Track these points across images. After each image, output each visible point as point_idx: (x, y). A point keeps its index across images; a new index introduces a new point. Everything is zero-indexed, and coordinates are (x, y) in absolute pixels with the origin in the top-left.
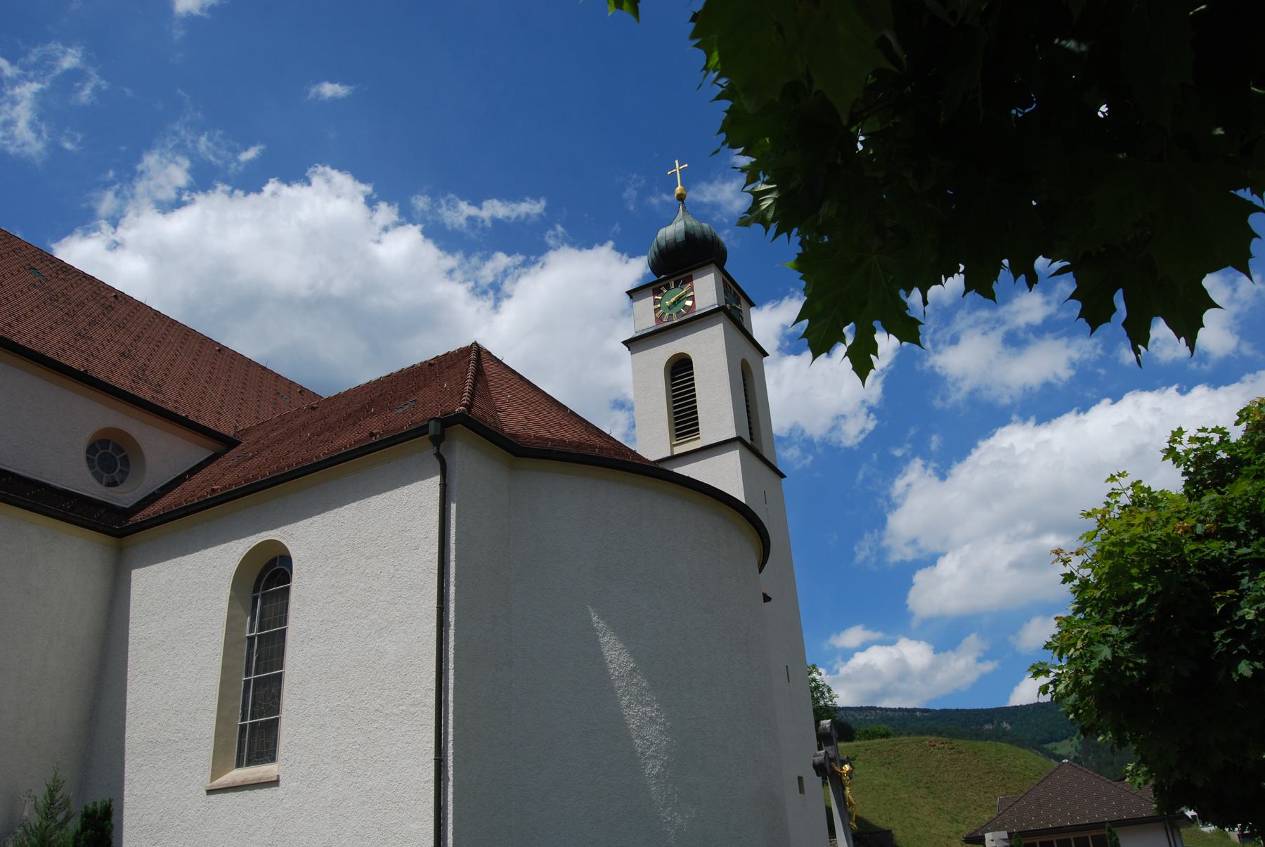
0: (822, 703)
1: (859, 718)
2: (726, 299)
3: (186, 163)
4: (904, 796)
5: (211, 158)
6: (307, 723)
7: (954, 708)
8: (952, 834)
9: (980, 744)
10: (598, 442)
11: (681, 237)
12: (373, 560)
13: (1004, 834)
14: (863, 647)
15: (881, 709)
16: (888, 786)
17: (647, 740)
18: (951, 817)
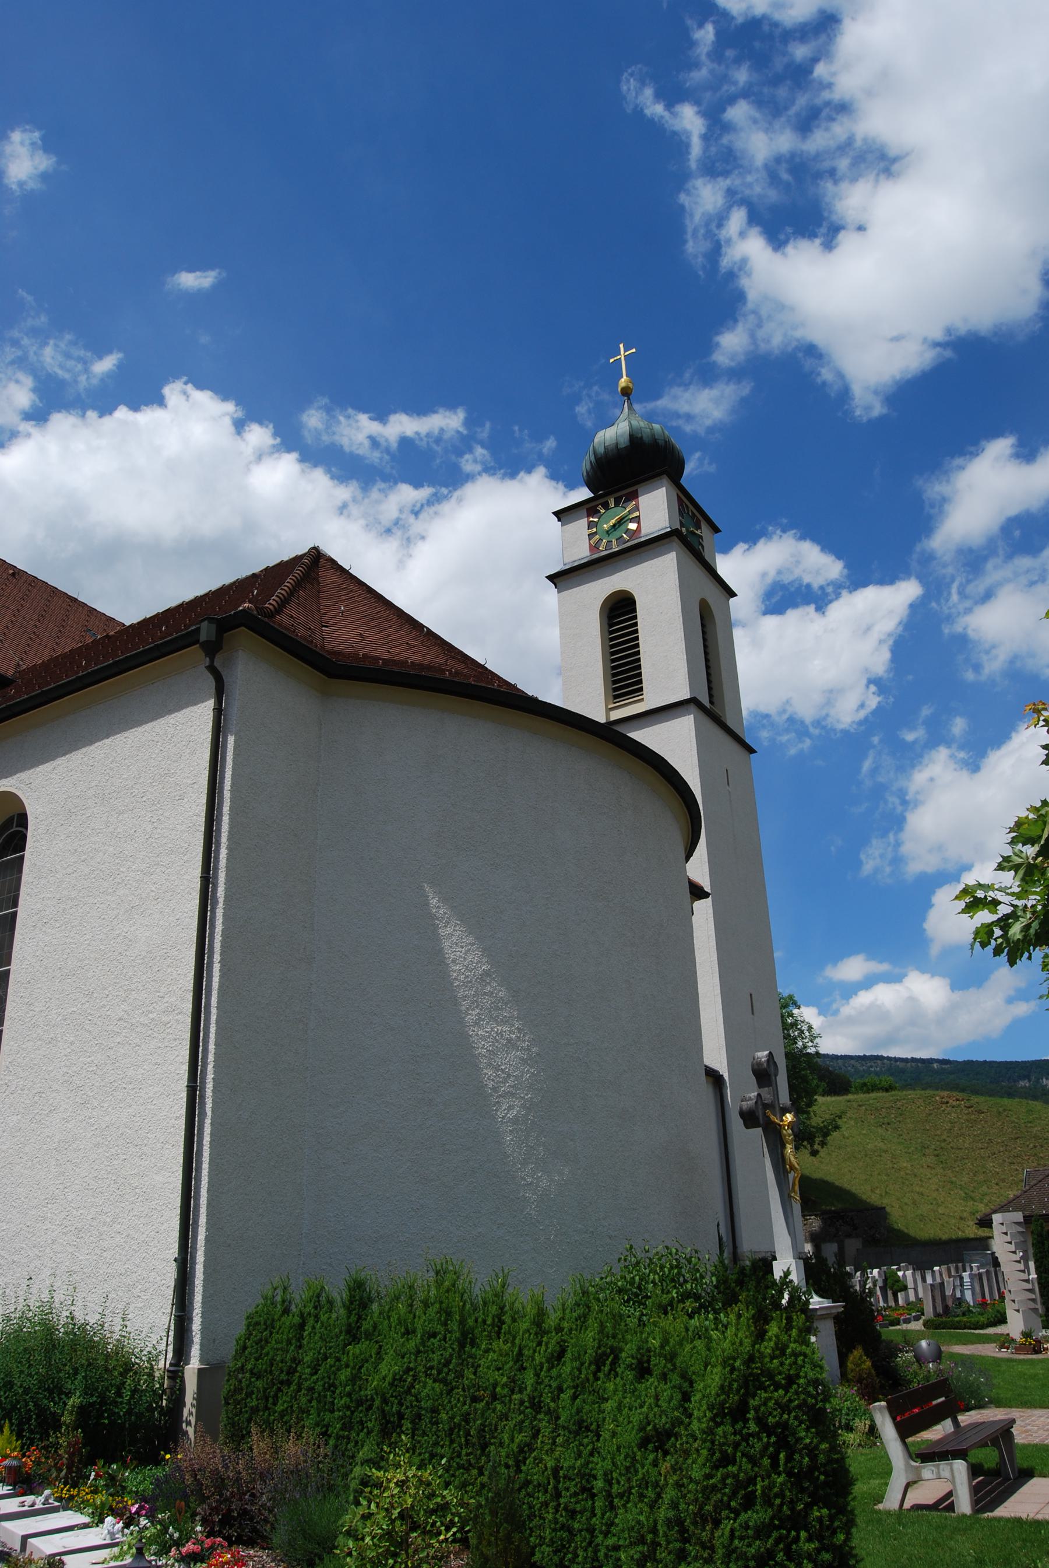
0: (800, 1044)
1: (861, 1069)
2: (681, 522)
3: (28, 381)
4: (905, 1165)
5: (60, 372)
6: (35, 1035)
7: (981, 1059)
8: (965, 1214)
9: (1006, 1101)
10: (454, 665)
11: (624, 442)
12: (126, 816)
13: (1019, 1216)
14: (868, 983)
15: (889, 1058)
16: (886, 1151)
17: (503, 1071)
18: (966, 1193)
